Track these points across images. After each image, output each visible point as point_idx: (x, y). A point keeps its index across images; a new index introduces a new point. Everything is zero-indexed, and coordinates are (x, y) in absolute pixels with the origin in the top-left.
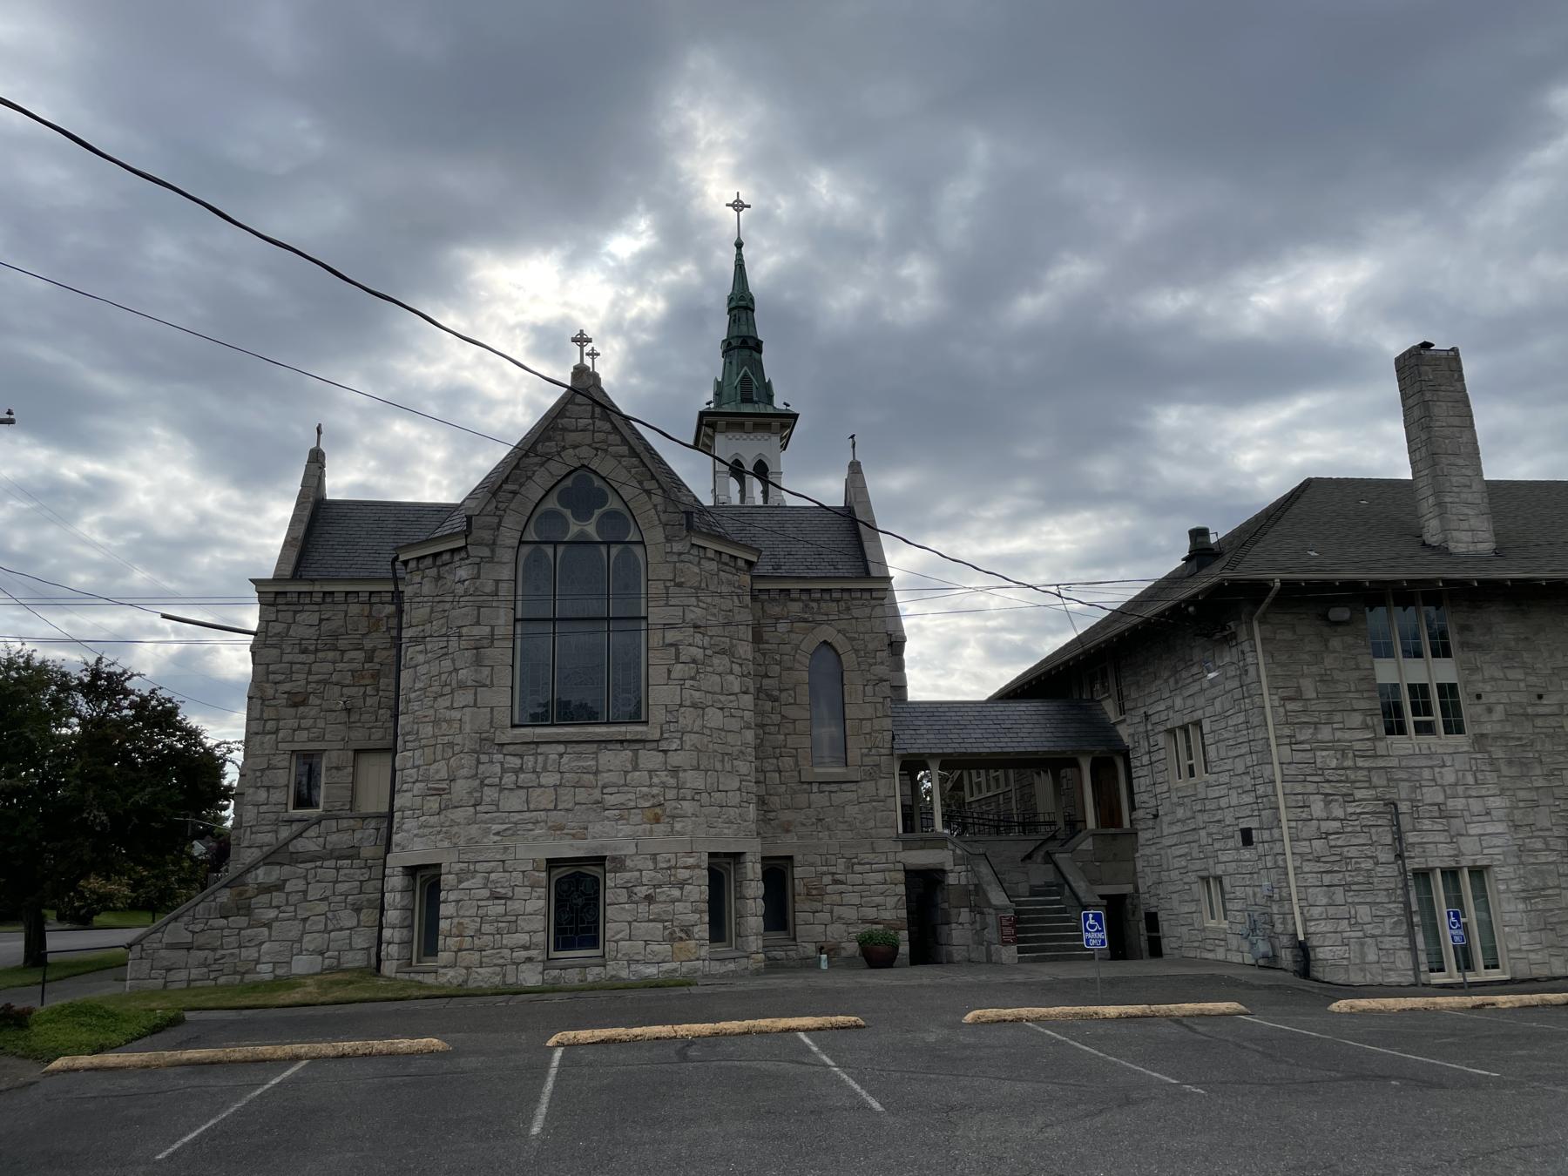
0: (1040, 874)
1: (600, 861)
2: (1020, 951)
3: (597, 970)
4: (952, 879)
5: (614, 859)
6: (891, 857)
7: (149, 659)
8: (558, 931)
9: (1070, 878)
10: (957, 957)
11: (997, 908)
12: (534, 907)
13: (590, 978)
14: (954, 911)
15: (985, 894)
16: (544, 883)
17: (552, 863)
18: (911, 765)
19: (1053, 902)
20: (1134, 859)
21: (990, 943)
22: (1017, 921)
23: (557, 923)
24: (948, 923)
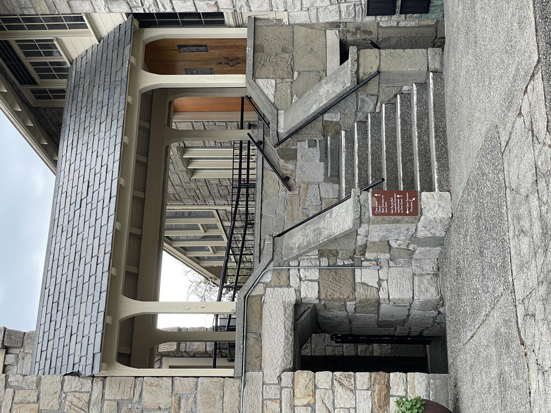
0: (309, 165)
2: (431, 189)
4: (310, 293)
6: (271, 392)
7: (351, 208)
9: (315, 108)
10: (432, 295)
11: (360, 220)
14: (360, 293)
15: (335, 240)
18: (134, 343)
19: (350, 140)
20: (291, 26)
21: (414, 239)
22: (376, 187)
24: (378, 303)
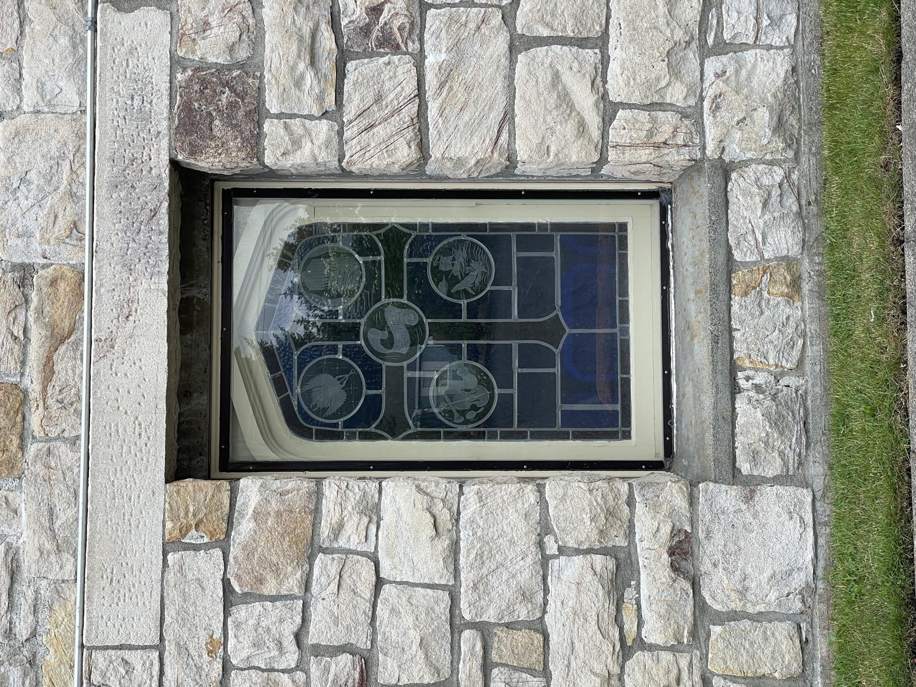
1: (200, 208)
3: (745, 208)
5: (189, 123)
8: (536, 420)
12: (410, 529)
13: (784, 241)
16: (296, 485)
17: (199, 447)
23: (491, 424)
